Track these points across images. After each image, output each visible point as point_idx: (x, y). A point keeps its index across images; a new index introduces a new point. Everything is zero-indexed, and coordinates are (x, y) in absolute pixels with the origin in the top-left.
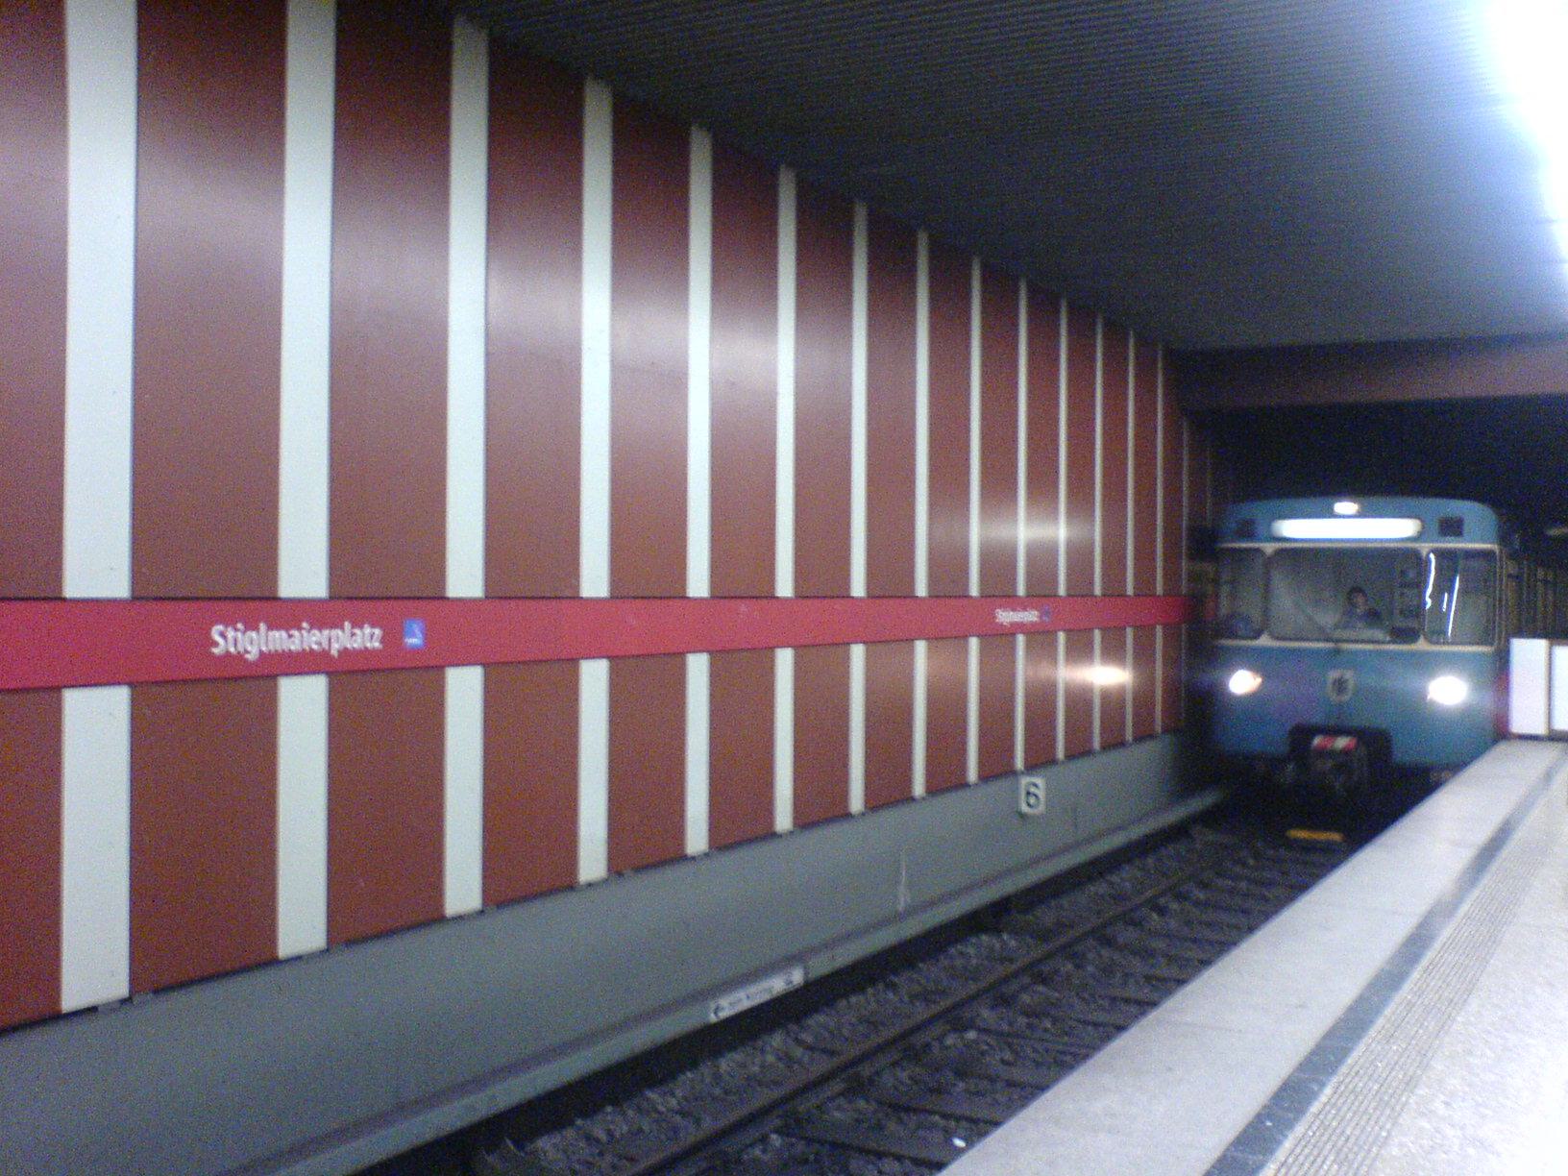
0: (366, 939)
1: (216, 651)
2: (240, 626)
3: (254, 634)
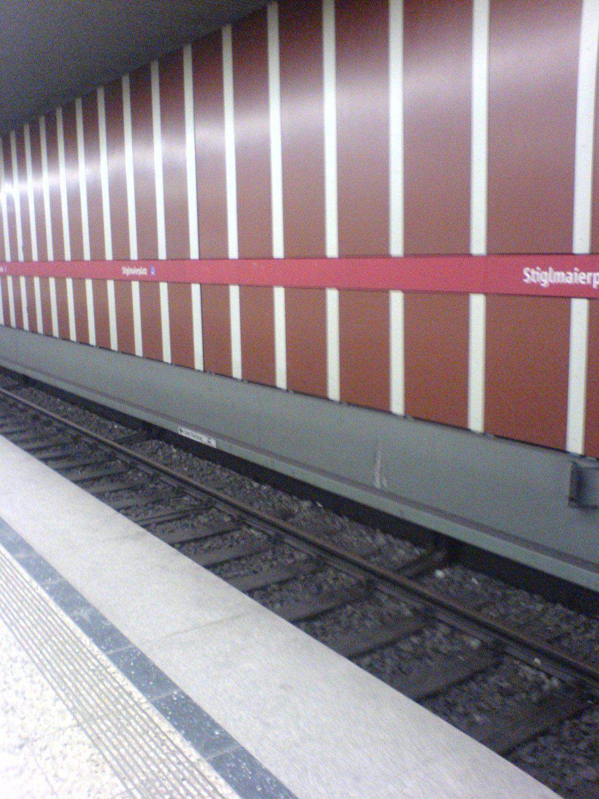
0: (354, 405)
1: (526, 281)
2: (538, 268)
3: (546, 273)
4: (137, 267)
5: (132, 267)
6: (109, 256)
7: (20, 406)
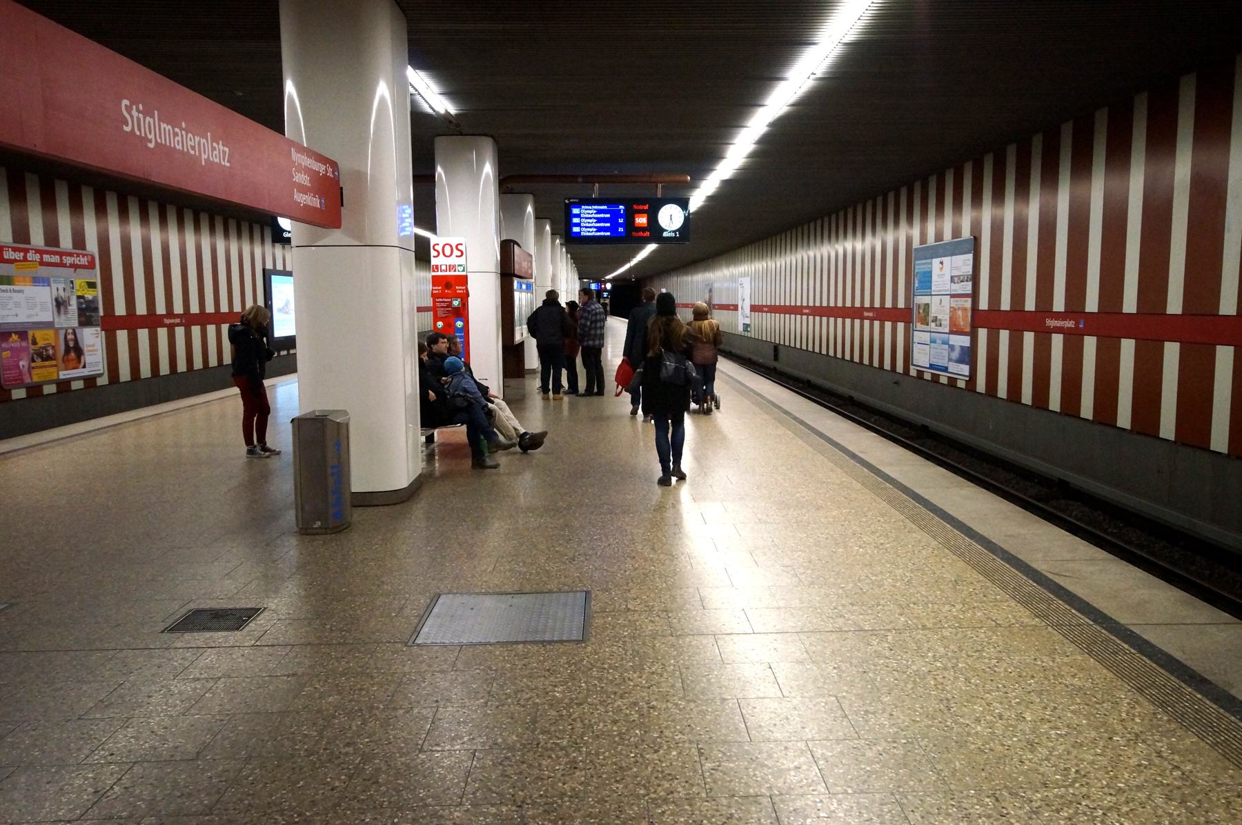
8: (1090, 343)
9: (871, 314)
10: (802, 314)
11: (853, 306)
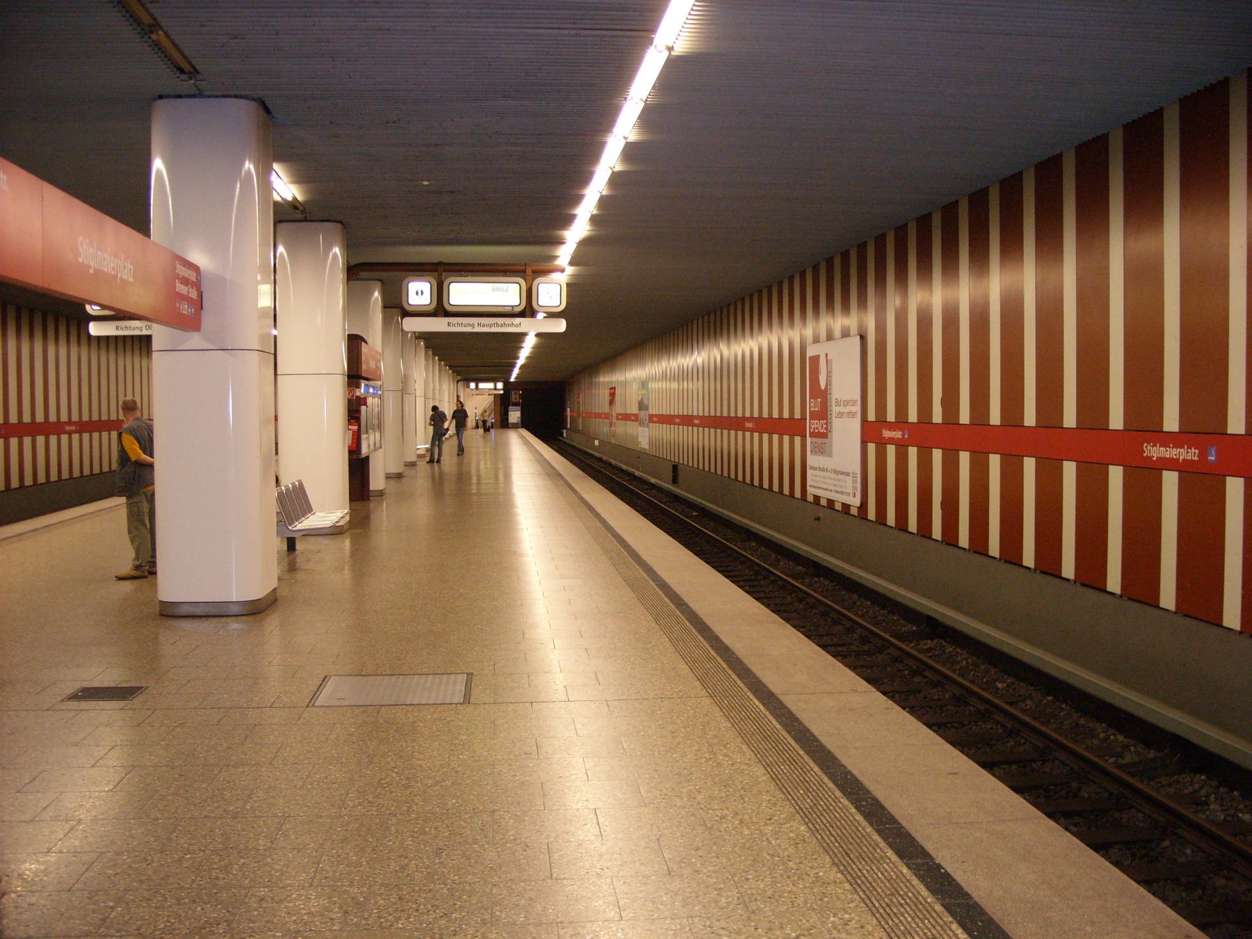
4: (1178, 445)
5: (1165, 445)
6: (1116, 420)
7: (810, 600)
8: (913, 452)
9: (897, 435)
10: (744, 430)
11: (771, 417)
